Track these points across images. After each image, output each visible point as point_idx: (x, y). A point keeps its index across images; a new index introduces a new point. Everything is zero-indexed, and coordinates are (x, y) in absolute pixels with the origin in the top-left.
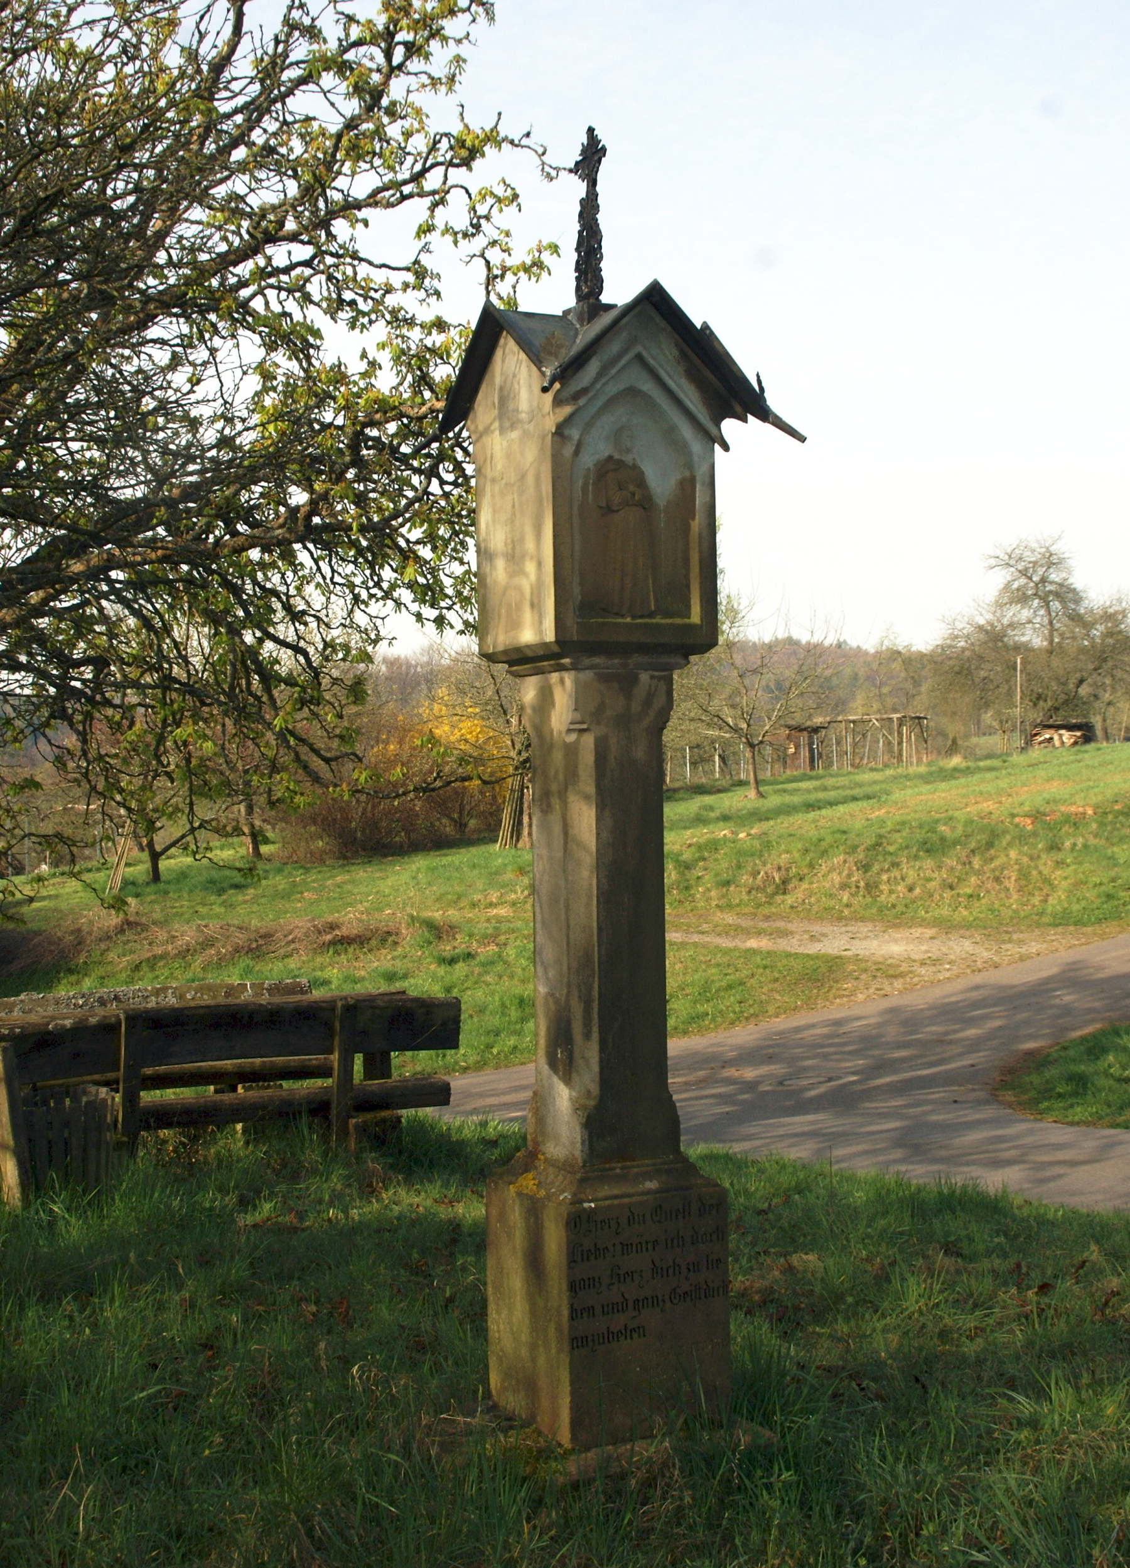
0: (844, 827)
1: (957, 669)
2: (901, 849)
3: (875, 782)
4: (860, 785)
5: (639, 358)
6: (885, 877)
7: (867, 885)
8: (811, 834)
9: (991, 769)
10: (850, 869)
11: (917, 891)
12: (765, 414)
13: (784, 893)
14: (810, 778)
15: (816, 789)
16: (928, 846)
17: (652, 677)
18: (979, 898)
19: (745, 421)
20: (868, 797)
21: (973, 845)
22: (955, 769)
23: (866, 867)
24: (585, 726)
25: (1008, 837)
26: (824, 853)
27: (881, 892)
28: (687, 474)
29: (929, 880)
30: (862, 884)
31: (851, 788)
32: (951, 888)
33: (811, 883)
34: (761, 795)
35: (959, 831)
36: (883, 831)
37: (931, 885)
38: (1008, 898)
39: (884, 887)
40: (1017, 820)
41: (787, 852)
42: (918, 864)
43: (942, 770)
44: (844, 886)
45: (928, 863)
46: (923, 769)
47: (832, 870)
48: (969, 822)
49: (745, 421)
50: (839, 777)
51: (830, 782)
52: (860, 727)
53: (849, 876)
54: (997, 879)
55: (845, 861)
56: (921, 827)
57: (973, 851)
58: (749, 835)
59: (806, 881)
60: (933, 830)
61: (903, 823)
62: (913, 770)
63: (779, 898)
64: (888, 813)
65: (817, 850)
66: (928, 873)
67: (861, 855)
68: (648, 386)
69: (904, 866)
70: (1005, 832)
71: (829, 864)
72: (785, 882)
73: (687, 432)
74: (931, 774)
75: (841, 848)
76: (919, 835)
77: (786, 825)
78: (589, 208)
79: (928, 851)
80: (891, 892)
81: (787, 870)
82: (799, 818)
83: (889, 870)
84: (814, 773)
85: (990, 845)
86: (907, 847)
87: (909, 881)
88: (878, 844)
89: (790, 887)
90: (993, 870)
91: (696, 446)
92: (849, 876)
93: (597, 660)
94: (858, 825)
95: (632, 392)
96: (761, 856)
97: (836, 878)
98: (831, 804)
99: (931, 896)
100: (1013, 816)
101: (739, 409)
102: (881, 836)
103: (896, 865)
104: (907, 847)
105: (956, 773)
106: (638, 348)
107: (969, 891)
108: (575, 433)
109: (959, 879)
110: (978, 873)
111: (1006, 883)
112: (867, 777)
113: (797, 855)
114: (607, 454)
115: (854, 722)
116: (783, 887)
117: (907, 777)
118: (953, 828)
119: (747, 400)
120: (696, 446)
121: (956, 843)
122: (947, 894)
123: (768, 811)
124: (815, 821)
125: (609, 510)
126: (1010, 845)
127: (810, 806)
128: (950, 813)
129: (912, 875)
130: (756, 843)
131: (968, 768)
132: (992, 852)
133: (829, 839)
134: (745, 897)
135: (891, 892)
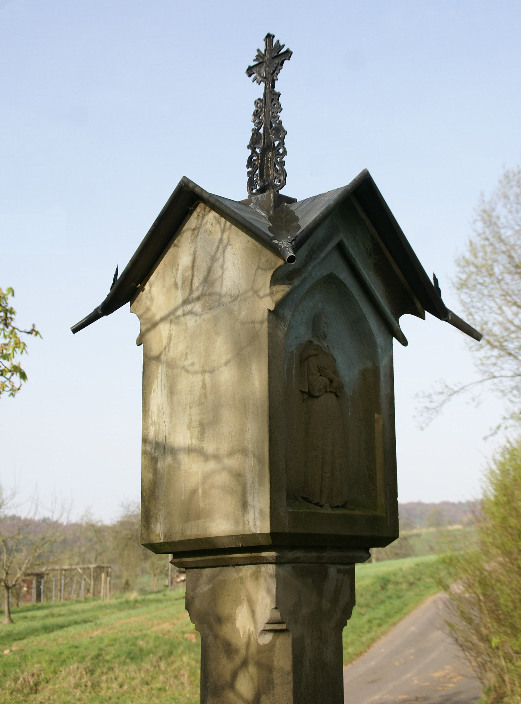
0: (76, 644)
1: (129, 536)
2: (115, 658)
3: (84, 611)
4: (76, 613)
5: (340, 247)
6: (104, 678)
7: (93, 684)
8: (54, 649)
9: (158, 601)
10: (81, 673)
11: (126, 687)
12: (442, 313)
13: (36, 693)
14: (39, 608)
15: (47, 616)
16: (132, 655)
17: (339, 571)
18: (165, 690)
19: (423, 317)
20: (85, 622)
21: (160, 654)
22: (136, 601)
23: (92, 672)
24: (283, 627)
25: (182, 647)
26: (64, 662)
27: (102, 688)
28: (370, 364)
29: (133, 679)
30: (89, 684)
31: (70, 615)
32: (147, 684)
33: (54, 684)
34: (11, 621)
35: (151, 645)
36: (102, 646)
37: (134, 683)
38: (183, 689)
39: (104, 685)
40: (186, 636)
41: (39, 663)
42: (126, 668)
43: (127, 602)
44: (77, 686)
45: (133, 667)
46: (113, 601)
47: (69, 674)
48: (157, 638)
49: (423, 317)
50: (58, 607)
51: (56, 611)
52: (69, 573)
53: (80, 678)
54: (176, 677)
55: (78, 668)
56: (127, 642)
57: (160, 658)
58: (11, 651)
59: (51, 682)
60: (134, 644)
61: (115, 640)
62: (108, 601)
63: (32, 697)
64: (103, 632)
65: (59, 660)
66: (133, 674)
67: (88, 663)
68: (344, 275)
69: (117, 670)
70: (179, 644)
71: (67, 670)
72: (36, 684)
73: (373, 323)
74: (121, 604)
75: (75, 658)
76: (126, 648)
77: (35, 643)
78: (268, 109)
79: (132, 659)
80: (108, 688)
81: (38, 676)
82: (43, 638)
83: (106, 673)
84: (39, 605)
85: (171, 653)
86: (118, 656)
87: (120, 680)
88: (99, 656)
89: (40, 688)
90: (173, 671)
91: (379, 338)
92: (80, 678)
93: (298, 554)
94: (85, 641)
95: (331, 280)
96: (20, 666)
97: (72, 680)
98: (61, 627)
99: (134, 690)
100: (184, 633)
101: (419, 305)
102: (101, 649)
103: (111, 669)
104: (118, 656)
105: (134, 605)
106: (342, 236)
107: (159, 686)
108: (287, 313)
109: (153, 678)
110: (164, 673)
111: (182, 679)
112: (79, 607)
113: (45, 665)
114: (306, 339)
115: (65, 570)
116: (35, 689)
117: (106, 607)
118: (147, 643)
119: (425, 298)
120: (379, 338)
121: (150, 652)
122: (145, 689)
123: (19, 633)
124: (55, 640)
125: (311, 395)
126: (183, 653)
127: (47, 629)
128: (144, 632)
129: (122, 676)
130: (17, 658)
131: (144, 600)
132: (172, 658)
133: (67, 652)
134: (8, 697)
135: (108, 688)
